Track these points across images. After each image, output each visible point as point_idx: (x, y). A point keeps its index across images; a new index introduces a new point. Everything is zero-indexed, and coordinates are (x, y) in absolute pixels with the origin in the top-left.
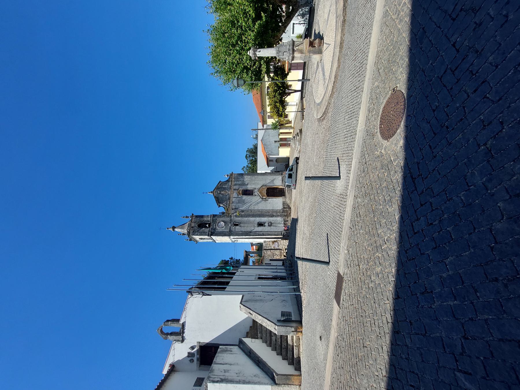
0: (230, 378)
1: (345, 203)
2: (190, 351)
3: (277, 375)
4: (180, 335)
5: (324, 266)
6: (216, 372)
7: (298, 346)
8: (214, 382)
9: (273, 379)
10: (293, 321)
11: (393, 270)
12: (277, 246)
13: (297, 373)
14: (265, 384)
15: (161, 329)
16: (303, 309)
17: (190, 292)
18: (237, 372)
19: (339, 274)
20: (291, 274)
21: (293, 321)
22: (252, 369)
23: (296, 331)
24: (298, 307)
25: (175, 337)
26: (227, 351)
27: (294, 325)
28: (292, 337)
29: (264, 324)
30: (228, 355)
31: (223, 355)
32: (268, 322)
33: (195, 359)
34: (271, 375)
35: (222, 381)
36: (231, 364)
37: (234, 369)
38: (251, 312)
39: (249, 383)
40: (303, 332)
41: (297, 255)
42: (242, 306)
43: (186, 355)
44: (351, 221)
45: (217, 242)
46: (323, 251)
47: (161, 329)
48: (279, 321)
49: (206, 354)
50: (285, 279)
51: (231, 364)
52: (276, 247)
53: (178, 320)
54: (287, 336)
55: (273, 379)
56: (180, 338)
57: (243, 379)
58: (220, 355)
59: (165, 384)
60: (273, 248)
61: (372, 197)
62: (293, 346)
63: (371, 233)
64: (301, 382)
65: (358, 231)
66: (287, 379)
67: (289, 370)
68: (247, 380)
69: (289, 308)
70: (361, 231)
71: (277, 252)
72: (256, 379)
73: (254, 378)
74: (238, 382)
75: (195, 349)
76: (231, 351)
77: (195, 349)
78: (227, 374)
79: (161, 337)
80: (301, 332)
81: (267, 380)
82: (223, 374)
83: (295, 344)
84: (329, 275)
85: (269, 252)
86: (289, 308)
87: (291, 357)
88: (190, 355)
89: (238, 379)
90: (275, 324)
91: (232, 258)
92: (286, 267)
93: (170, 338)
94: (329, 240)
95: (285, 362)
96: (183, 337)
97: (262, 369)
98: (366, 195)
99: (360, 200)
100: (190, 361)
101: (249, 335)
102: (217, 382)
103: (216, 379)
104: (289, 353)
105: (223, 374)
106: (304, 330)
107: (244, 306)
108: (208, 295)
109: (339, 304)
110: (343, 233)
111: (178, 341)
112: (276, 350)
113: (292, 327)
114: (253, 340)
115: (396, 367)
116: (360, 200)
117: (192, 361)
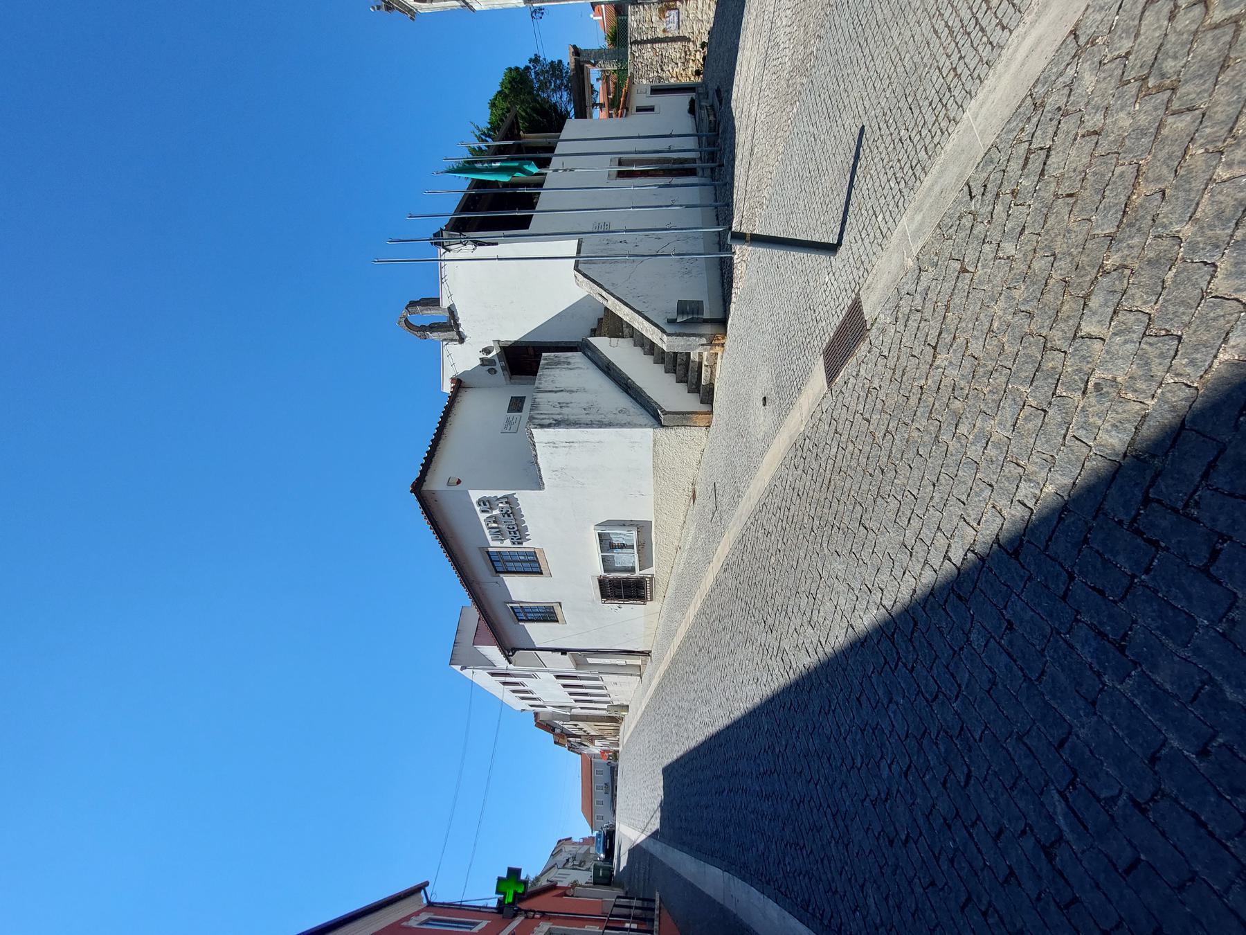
0: (572, 418)
1: (998, 36)
2: (483, 356)
3: (665, 413)
4: (451, 326)
5: (822, 258)
6: (545, 408)
7: (712, 367)
8: (542, 426)
9: (656, 417)
10: (706, 321)
11: (1050, 489)
12: (673, 26)
13: (704, 408)
14: (641, 426)
15: (406, 320)
16: (734, 299)
17: (438, 240)
18: (585, 406)
19: (856, 309)
20: (713, 154)
21: (706, 321)
22: (614, 399)
23: (710, 344)
24: (722, 276)
25: (443, 335)
26: (559, 363)
27: (707, 329)
28: (700, 355)
29: (636, 326)
30: (564, 372)
31: (553, 372)
32: (646, 323)
33: (498, 367)
34: (654, 414)
35: (558, 424)
36: (571, 392)
37: (580, 399)
38: (604, 293)
39: (610, 425)
40: (727, 347)
41: (735, 227)
42: (580, 276)
43: (479, 362)
44: (987, 159)
45: (477, 7)
46: (826, 181)
47: (406, 320)
48: (672, 322)
49: (521, 360)
50: (691, 172)
51: (571, 392)
52: (673, 32)
53: (435, 302)
54: (688, 354)
55: (656, 417)
56: (453, 334)
57: (599, 418)
58: (546, 372)
59: (454, 411)
60: (661, 35)
61: (1179, 125)
62: (700, 364)
63: (1049, 297)
64: (710, 422)
65: (996, 235)
66: (683, 418)
67: (689, 402)
68: (606, 421)
69: (698, 289)
70: (1009, 248)
71: (675, 51)
72: (624, 418)
73: (620, 416)
74: (590, 425)
75: (494, 353)
76: (569, 363)
77: (494, 353)
78: (565, 410)
79: (412, 337)
80: (723, 345)
81: (645, 418)
82: (559, 410)
83: (705, 363)
84: (824, 287)
85: (648, 53)
86: (698, 289)
87: (694, 381)
88: (484, 362)
89: (587, 419)
90: (663, 331)
91: (536, 60)
92: (700, 137)
93: (434, 336)
94: (862, 162)
95: (682, 387)
96: (459, 333)
97: (635, 399)
98: (1152, 81)
99: (1089, 80)
100: (489, 371)
101: (604, 329)
102: (549, 426)
103: (547, 422)
104: (692, 376)
105: (559, 410)
106: (728, 342)
107: (585, 276)
108: (489, 244)
109: (831, 376)
110: (927, 181)
111: (452, 340)
112: (663, 362)
113: (701, 336)
114: (614, 340)
115: (919, 626)
116: (1089, 80)
117: (492, 371)
